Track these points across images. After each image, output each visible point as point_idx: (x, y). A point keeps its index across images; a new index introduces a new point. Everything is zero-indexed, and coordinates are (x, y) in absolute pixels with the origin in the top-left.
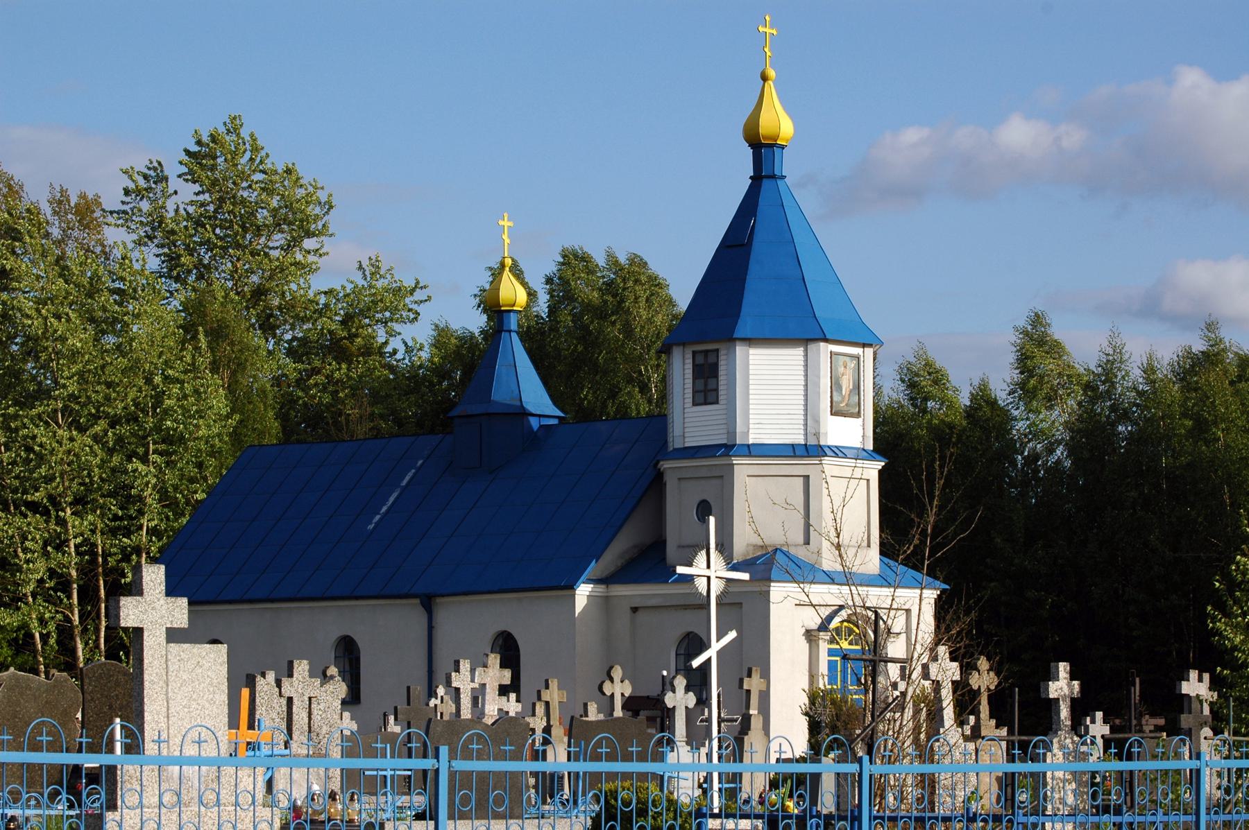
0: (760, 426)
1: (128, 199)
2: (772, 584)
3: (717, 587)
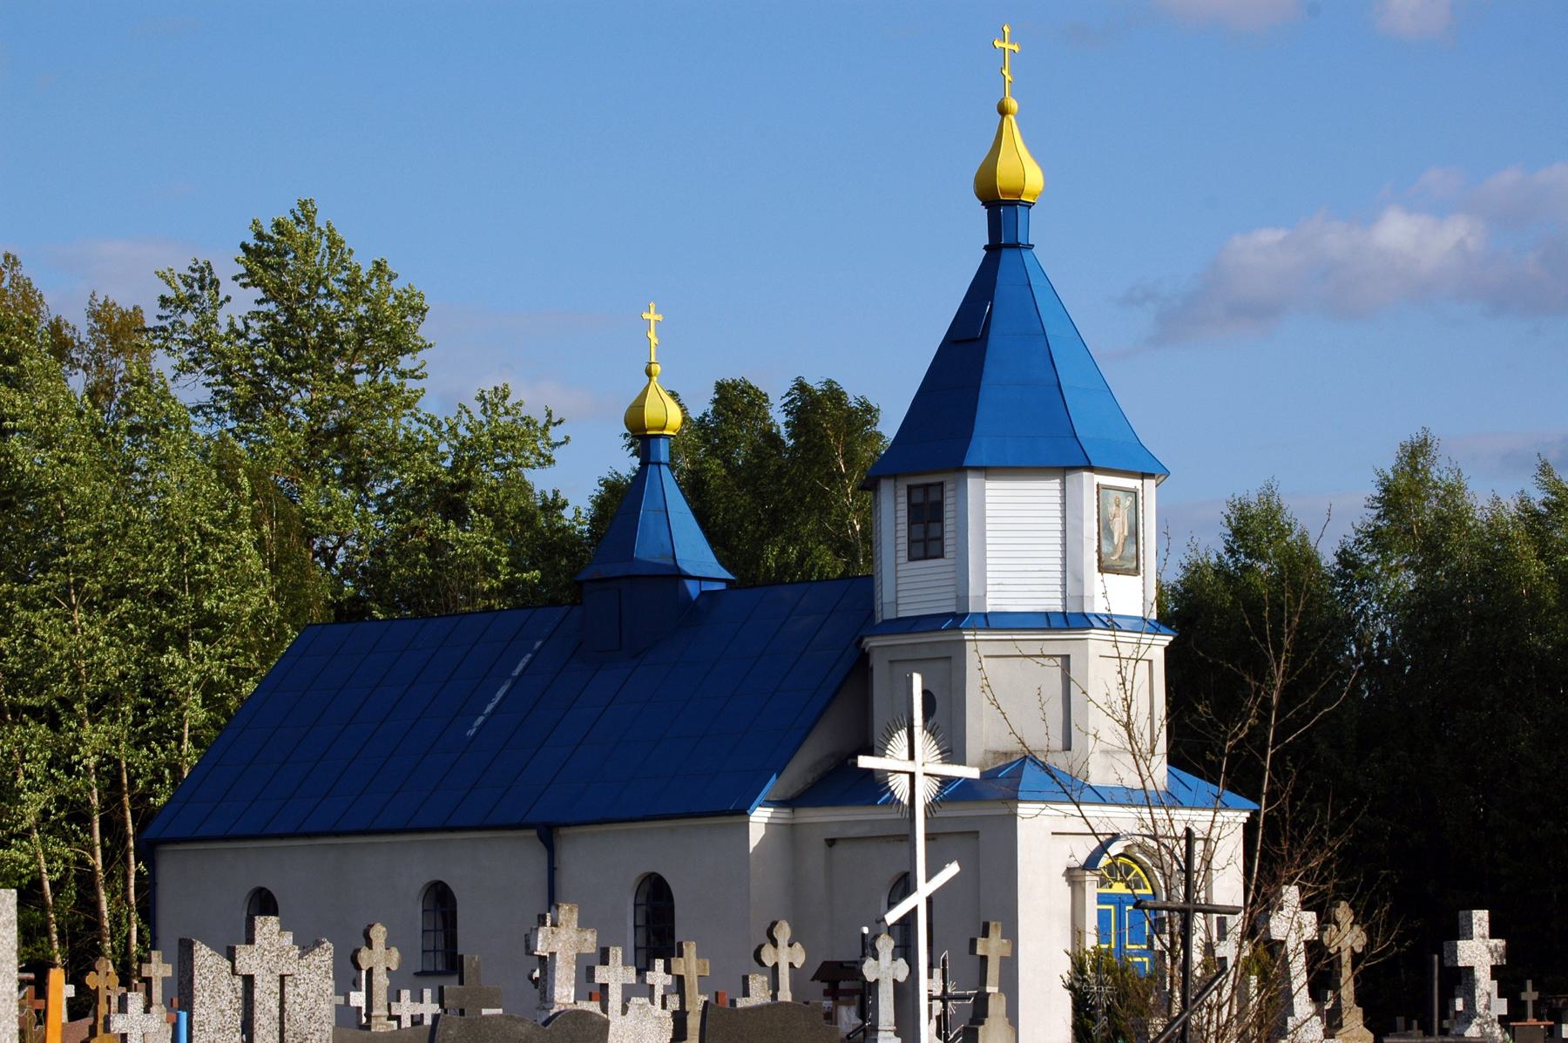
0: (1001, 588)
1: (166, 313)
2: (1020, 805)
3: (925, 791)
